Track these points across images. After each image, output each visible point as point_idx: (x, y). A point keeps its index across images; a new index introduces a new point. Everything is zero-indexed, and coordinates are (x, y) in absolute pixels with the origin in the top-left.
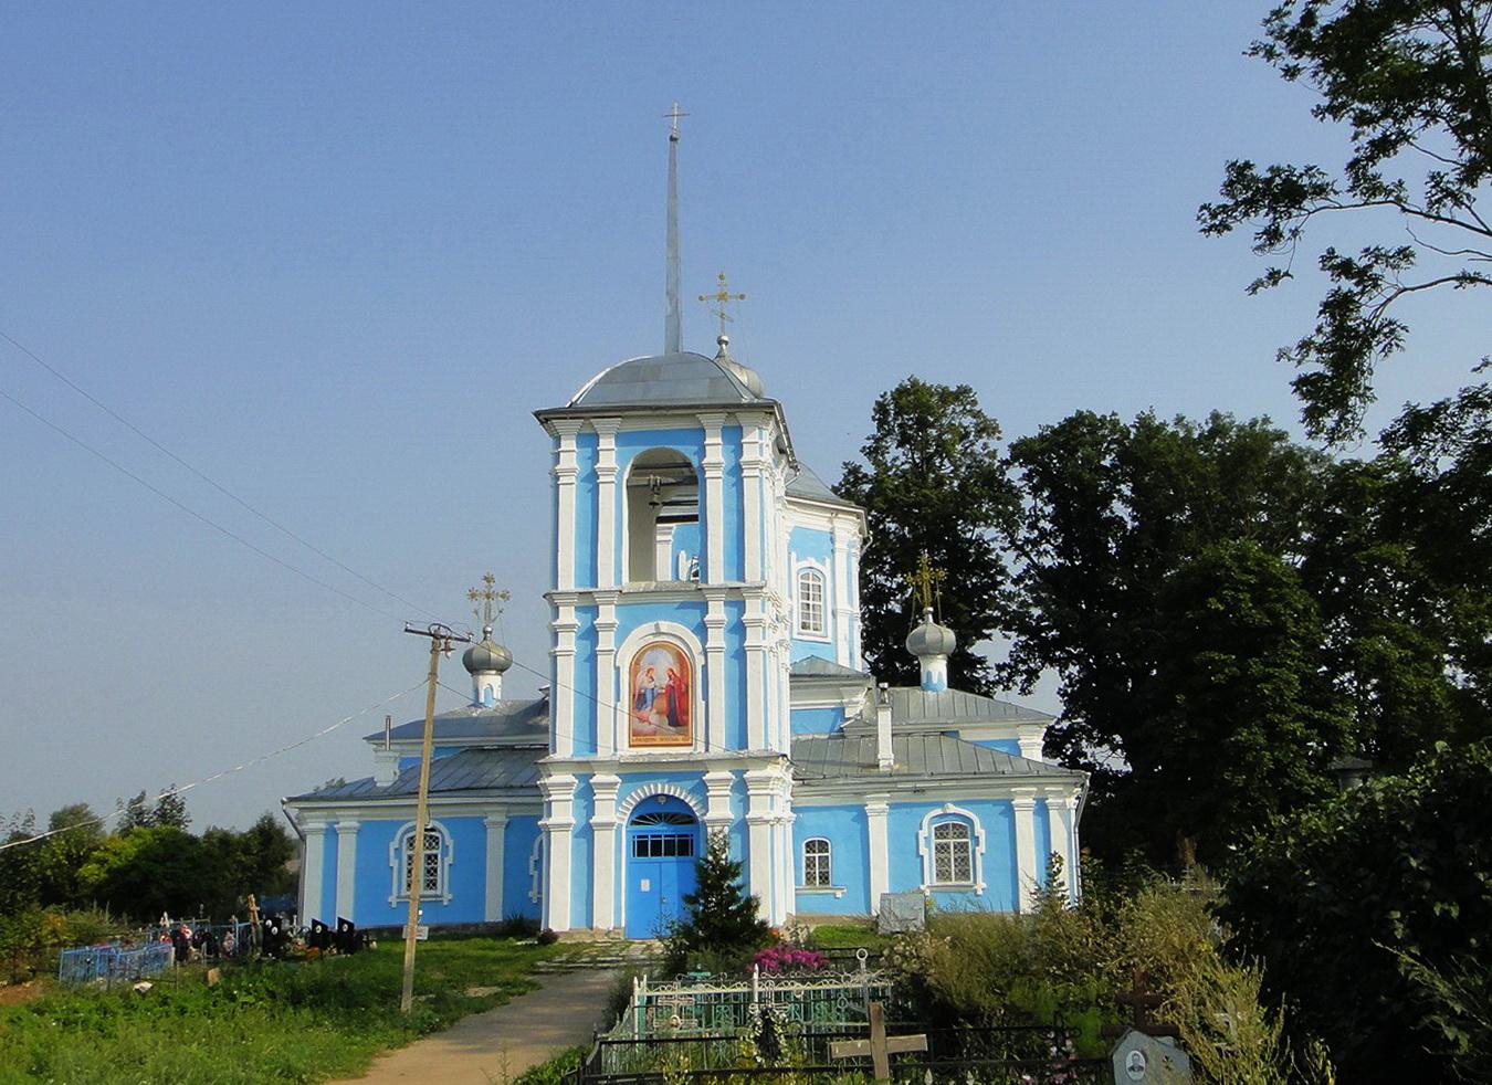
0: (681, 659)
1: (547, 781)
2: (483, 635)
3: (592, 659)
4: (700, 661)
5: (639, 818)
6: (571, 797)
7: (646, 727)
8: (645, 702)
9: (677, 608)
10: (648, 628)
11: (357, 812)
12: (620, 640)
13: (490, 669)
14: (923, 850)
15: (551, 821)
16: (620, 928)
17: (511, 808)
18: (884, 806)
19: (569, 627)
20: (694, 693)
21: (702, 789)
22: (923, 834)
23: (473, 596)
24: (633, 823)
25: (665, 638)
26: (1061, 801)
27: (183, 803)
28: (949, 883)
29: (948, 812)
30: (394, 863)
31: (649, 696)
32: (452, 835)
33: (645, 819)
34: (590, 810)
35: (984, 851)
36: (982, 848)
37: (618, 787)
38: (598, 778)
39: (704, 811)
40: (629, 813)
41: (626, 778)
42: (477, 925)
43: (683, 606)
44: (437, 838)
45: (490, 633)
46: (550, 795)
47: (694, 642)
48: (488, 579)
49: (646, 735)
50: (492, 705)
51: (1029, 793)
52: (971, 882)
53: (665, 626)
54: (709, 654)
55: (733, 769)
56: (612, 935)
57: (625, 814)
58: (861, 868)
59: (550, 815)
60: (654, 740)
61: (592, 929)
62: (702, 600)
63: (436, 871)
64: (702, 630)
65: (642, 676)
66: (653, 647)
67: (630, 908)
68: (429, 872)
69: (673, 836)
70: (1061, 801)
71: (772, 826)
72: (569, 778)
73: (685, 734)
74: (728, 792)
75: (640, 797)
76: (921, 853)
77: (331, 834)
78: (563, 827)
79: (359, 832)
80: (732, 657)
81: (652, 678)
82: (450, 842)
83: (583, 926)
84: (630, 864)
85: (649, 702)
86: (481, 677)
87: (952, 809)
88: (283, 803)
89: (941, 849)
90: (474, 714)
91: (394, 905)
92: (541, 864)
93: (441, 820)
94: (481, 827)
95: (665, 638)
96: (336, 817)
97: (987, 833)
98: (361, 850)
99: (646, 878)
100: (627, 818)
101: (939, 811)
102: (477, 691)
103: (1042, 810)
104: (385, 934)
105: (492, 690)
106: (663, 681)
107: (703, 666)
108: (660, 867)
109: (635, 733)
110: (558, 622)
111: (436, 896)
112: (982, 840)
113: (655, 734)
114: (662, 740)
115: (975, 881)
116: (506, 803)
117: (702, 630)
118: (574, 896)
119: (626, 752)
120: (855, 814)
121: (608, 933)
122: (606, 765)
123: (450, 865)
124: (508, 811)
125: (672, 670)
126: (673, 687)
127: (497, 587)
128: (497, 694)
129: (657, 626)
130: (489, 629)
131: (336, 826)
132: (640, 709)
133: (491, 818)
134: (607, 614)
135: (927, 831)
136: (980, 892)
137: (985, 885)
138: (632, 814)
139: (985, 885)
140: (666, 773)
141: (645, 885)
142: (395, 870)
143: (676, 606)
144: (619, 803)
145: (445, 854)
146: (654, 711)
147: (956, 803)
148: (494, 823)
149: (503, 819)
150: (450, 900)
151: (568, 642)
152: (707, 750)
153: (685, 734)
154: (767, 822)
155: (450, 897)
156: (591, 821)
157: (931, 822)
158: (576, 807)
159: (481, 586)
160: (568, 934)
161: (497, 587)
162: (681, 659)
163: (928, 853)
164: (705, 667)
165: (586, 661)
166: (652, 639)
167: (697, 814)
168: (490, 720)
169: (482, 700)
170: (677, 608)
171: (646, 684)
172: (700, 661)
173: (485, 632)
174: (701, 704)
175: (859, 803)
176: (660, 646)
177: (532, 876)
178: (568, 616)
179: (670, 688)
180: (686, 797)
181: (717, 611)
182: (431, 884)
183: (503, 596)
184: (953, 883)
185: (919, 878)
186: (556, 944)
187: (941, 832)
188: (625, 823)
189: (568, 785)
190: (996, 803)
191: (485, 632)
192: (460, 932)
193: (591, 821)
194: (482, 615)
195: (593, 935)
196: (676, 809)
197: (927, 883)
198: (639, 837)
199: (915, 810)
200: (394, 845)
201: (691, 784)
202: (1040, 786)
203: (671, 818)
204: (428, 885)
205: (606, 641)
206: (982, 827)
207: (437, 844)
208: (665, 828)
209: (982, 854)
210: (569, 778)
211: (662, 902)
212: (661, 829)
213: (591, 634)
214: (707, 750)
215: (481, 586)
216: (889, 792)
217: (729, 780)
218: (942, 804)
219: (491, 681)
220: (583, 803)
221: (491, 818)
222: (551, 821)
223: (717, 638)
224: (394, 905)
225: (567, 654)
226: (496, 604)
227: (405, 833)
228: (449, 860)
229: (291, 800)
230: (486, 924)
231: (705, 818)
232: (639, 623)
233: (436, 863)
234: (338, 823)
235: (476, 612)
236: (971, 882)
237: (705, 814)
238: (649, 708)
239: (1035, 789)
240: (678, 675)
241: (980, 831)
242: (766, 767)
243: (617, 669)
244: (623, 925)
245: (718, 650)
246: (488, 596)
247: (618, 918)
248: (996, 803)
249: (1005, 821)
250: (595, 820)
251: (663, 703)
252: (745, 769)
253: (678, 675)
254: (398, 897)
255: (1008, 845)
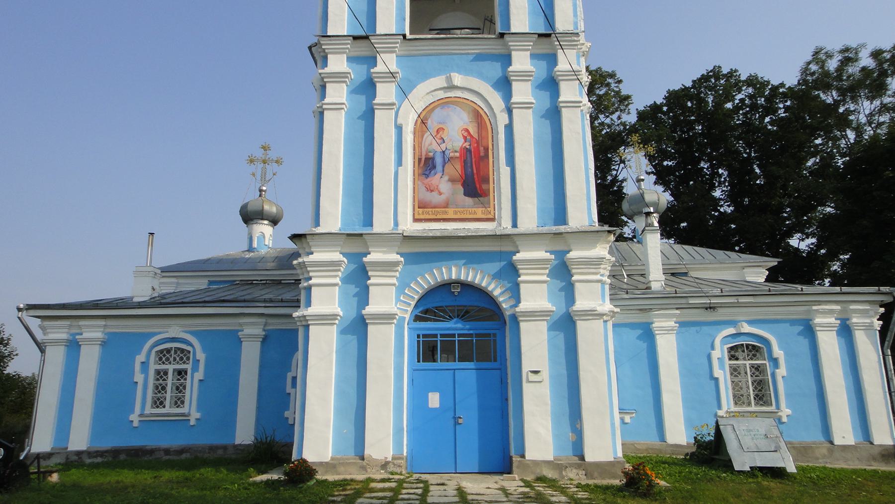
0: (478, 117)
1: (306, 259)
2: (259, 193)
3: (369, 116)
4: (502, 119)
5: (426, 312)
6: (337, 280)
7: (435, 198)
8: (434, 167)
9: (472, 61)
10: (439, 81)
11: (102, 322)
12: (404, 93)
13: (262, 219)
14: (718, 373)
15: (311, 311)
16: (401, 458)
17: (270, 321)
18: (672, 323)
19: (339, 77)
20: (496, 158)
21: (510, 273)
22: (716, 354)
23: (252, 161)
24: (417, 318)
25: (459, 94)
26: (868, 321)
27: (9, 339)
28: (749, 409)
29: (743, 331)
30: (139, 378)
31: (439, 160)
32: (204, 349)
33: (444, 311)
34: (363, 297)
35: (785, 374)
36: (782, 371)
37: (399, 268)
38: (375, 256)
39: (512, 302)
40: (413, 303)
41: (413, 259)
42: (225, 448)
43: (480, 57)
44: (189, 352)
45: (265, 191)
46: (310, 278)
47: (496, 100)
48: (265, 148)
49: (435, 207)
50: (263, 251)
51: (831, 312)
52: (773, 408)
53: (458, 79)
54: (514, 111)
55: (549, 249)
56: (391, 468)
57: (410, 304)
58: (649, 391)
59: (309, 304)
60: (446, 213)
61: (363, 458)
62: (503, 51)
63: (185, 388)
64: (504, 85)
65: (428, 139)
66: (444, 103)
67: (412, 430)
68: (177, 388)
69: (470, 335)
70: (868, 321)
71: (605, 322)
72: (336, 256)
73: (486, 205)
74: (545, 278)
75: (423, 288)
76: (716, 375)
77: (73, 346)
78: (326, 319)
79: (104, 344)
80: (542, 117)
81: (442, 138)
82: (201, 356)
83: (351, 453)
84: (413, 371)
85: (439, 167)
86: (255, 225)
87: (747, 328)
88: (19, 310)
89: (735, 371)
90: (247, 256)
91: (136, 424)
92: (298, 382)
93: (191, 333)
94: (235, 340)
95: (459, 94)
96: (80, 327)
97: (786, 354)
98: (104, 363)
99: (434, 390)
100: (410, 309)
101: (731, 331)
102: (251, 239)
103: (846, 331)
104: (122, 457)
105: (264, 237)
106: (455, 142)
107: (506, 126)
108: (454, 372)
109: (421, 205)
110: (327, 70)
111: (183, 415)
112: (782, 362)
113: (446, 205)
114: (455, 213)
115: (778, 407)
116: (262, 315)
117: (504, 85)
118: (339, 411)
119: (409, 226)
120: (639, 332)
121: (385, 465)
122: (384, 239)
123: (200, 380)
124: (265, 325)
125: (467, 130)
126: (469, 151)
127: (272, 155)
128: (268, 242)
129: (449, 79)
130: (264, 188)
131: (77, 337)
132: (427, 176)
133: (248, 331)
134: (387, 62)
135: (719, 352)
136: (785, 419)
137: (789, 412)
138: (416, 306)
139: (789, 412)
140: (463, 253)
141: (434, 400)
142: (140, 388)
143: (471, 57)
144: (400, 290)
145: (195, 369)
146: (446, 178)
147: (751, 322)
148: (251, 336)
149: (259, 331)
150: (197, 419)
151: (337, 93)
152: (515, 225)
153: (486, 205)
154: (601, 315)
155: (198, 415)
156: (364, 312)
157: (723, 341)
158: (343, 294)
159: (259, 154)
160: (330, 466)
161: (272, 155)
162: (478, 117)
163: (722, 374)
164: (509, 128)
165: (359, 118)
166: (441, 95)
167: (504, 306)
168: (262, 259)
169: (255, 245)
170: (472, 61)
171: (435, 146)
172: (502, 119)
173: (261, 191)
174: (505, 171)
175: (644, 320)
176: (453, 103)
177: (289, 394)
178: (337, 63)
179: (465, 152)
180: (489, 284)
181: (521, 61)
182: (179, 402)
183: (277, 162)
184: (753, 408)
185: (715, 402)
186: (312, 483)
187: (733, 352)
188: (407, 316)
189: (333, 265)
190: (793, 322)
191: (261, 191)
192: (206, 456)
193: (364, 312)
194: (259, 178)
195: (364, 468)
196: (467, 301)
197: (725, 407)
198: (424, 336)
199: (705, 329)
200: (140, 358)
201: (496, 266)
202: (845, 305)
203: (464, 314)
204: (176, 403)
205: (385, 92)
206: (781, 348)
207: (188, 359)
208: (459, 325)
209: (783, 377)
210: (335, 256)
211: (456, 423)
212: (454, 326)
213: (368, 87)
214: (515, 225)
215: (259, 154)
216: (677, 309)
217: (547, 260)
218: (733, 323)
219: (264, 229)
220: (353, 289)
221: (248, 331)
222: (311, 311)
223: (522, 92)
224: (136, 424)
225: (337, 107)
226: (271, 168)
227: (157, 344)
228: (199, 375)
229: (31, 307)
230: (236, 447)
231: (518, 309)
232: (426, 76)
233: (185, 379)
234: (81, 334)
235: (254, 175)
236: (773, 408)
237: (516, 306)
238: (439, 175)
239: (838, 307)
240: (476, 136)
241: (778, 352)
242: (595, 247)
243: (399, 129)
244: (405, 454)
245: (526, 106)
246: (264, 162)
247: (398, 443)
248: (793, 322)
249: (804, 343)
250: (369, 310)
251: (455, 169)
252: (566, 249)
253: (476, 136)
254: (141, 415)
255: (810, 365)
